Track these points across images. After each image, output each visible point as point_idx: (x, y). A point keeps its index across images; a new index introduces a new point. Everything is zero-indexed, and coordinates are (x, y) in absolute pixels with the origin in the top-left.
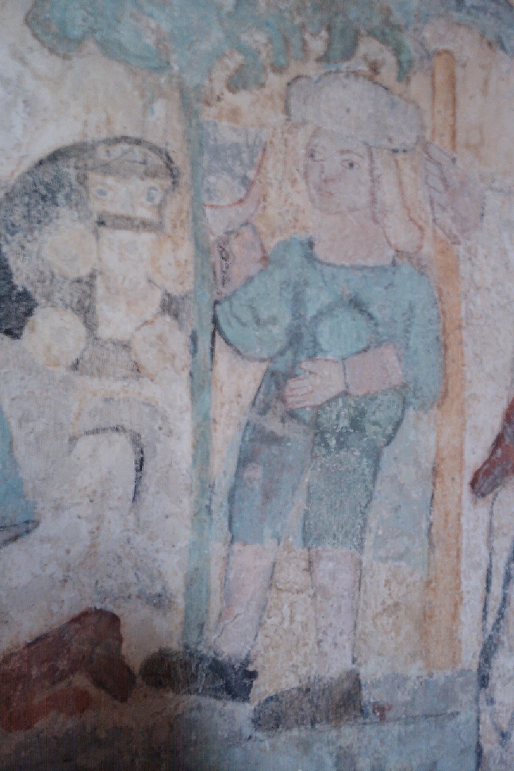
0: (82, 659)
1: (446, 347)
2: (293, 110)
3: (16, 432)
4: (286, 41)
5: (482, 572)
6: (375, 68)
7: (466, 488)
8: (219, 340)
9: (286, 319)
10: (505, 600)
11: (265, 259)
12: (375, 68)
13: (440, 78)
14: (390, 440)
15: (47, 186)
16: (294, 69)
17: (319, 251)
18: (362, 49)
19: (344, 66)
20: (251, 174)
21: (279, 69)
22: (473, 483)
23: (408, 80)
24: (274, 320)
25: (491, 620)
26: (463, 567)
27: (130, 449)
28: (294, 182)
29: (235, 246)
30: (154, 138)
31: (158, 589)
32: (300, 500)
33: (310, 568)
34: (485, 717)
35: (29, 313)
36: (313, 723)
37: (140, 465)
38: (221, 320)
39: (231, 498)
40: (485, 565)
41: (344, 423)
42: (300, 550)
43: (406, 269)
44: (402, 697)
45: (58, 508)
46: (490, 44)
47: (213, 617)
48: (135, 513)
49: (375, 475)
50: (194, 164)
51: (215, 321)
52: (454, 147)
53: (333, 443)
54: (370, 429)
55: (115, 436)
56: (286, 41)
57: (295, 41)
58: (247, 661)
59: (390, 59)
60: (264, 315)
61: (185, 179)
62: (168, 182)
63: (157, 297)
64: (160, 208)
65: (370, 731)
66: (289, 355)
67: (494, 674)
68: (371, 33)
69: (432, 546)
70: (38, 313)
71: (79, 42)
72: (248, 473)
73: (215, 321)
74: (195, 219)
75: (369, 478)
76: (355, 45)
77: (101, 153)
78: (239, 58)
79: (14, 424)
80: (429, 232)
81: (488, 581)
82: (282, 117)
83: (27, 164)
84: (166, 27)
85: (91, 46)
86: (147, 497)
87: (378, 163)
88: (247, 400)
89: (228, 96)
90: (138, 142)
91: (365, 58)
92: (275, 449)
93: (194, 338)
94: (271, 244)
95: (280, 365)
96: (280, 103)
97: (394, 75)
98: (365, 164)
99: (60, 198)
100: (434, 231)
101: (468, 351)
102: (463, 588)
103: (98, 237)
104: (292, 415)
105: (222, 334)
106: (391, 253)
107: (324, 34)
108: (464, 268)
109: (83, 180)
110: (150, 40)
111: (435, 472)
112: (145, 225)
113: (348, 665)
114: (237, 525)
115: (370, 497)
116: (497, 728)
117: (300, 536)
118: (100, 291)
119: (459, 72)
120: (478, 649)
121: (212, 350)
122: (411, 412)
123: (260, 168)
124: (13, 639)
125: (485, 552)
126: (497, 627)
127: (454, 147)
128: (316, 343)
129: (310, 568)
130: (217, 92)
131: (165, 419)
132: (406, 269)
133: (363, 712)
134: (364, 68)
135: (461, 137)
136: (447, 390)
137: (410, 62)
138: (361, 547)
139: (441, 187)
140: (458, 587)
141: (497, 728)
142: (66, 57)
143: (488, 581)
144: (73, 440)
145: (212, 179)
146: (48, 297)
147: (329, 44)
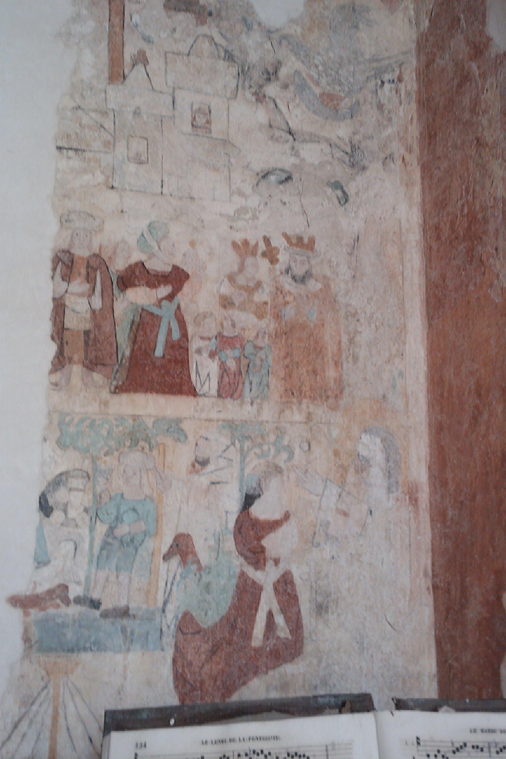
0: (367, 57)
1: (158, 521)
2: (121, 460)
3: (47, 540)
4: (120, 443)
5: (165, 582)
6: (143, 449)
7: (162, 558)
8: (97, 518)
9: (115, 513)
10: (171, 589)
11: (110, 498)
12: (143, 449)
13: (161, 450)
14: (140, 545)
15: (58, 482)
16: (121, 450)
17: (125, 496)
18: (140, 444)
19: (135, 448)
20: (108, 477)
21: (117, 450)
22: (163, 558)
23: (152, 451)
24: (112, 514)
25: (167, 594)
26: (159, 580)
27: (73, 544)
28: (119, 478)
29: (103, 495)
30: (85, 469)
31: (78, 580)
32: (116, 560)
33: (117, 577)
34: (164, 622)
35: (52, 511)
36: (115, 617)
37: (76, 549)
38: (98, 514)
39: (98, 559)
40: (165, 580)
41: (129, 540)
42: (115, 572)
43: (148, 500)
44: (140, 613)
45: (55, 558)
46: (176, 441)
47: (92, 587)
48: (22, 676)
49: (136, 554)
50: (94, 475)
51: (97, 514)
52: (164, 468)
53: (125, 545)
54: (135, 542)
55: (70, 542)
56: (120, 443)
57: (122, 443)
58: (99, 600)
59: (148, 446)
60: (109, 512)
61: (91, 479)
62: (87, 479)
63: (82, 508)
64: (85, 486)
65: (131, 621)
66: (115, 523)
67: (166, 610)
68: (143, 440)
69: (151, 573)
70: (54, 512)
71: (68, 447)
72: (103, 552)
73: (97, 514)
74: (94, 488)
75: (134, 554)
76: (138, 442)
77: (72, 473)
78: (107, 448)
79: (47, 538)
80: (155, 491)
81: (166, 584)
82: (118, 462)
83: (54, 476)
84: (89, 442)
85: (71, 447)
86: (77, 557)
87: (143, 473)
88: (104, 533)
89: (104, 458)
90: (81, 470)
91: (141, 446)
92: (110, 546)
93: (91, 519)
94: (112, 495)
95: (113, 525)
96: (117, 459)
97: (148, 450)
98: (139, 474)
99: (61, 484)
100: (157, 491)
101: (164, 523)
102: (159, 585)
103: (69, 493)
104: (115, 538)
105: (98, 517)
106: (144, 496)
107: (130, 441)
108: (164, 500)
109: (67, 479)
110: (85, 445)
111: (153, 554)
112: (81, 490)
113: (126, 603)
114: (99, 565)
115: (134, 559)
116: (167, 624)
117: (115, 568)
118: (69, 505)
119: (166, 448)
120: (162, 602)
121: (95, 522)
122: (147, 538)
123: (111, 475)
124: (140, 613)
125: (166, 576)
126: (168, 596)
127: (164, 468)
128: (122, 519)
129: (117, 577)
130: (101, 456)
131: (82, 537)
132: (148, 500)
133: (129, 615)
134: (141, 449)
135: (166, 466)
136: (157, 532)
137: (153, 447)
138: (131, 573)
139: (159, 478)
140: (158, 584)
141: (167, 624)
142: (65, 450)
143: (166, 584)
144: (60, 542)
145: (98, 478)
146: (57, 508)
147: (131, 444)
